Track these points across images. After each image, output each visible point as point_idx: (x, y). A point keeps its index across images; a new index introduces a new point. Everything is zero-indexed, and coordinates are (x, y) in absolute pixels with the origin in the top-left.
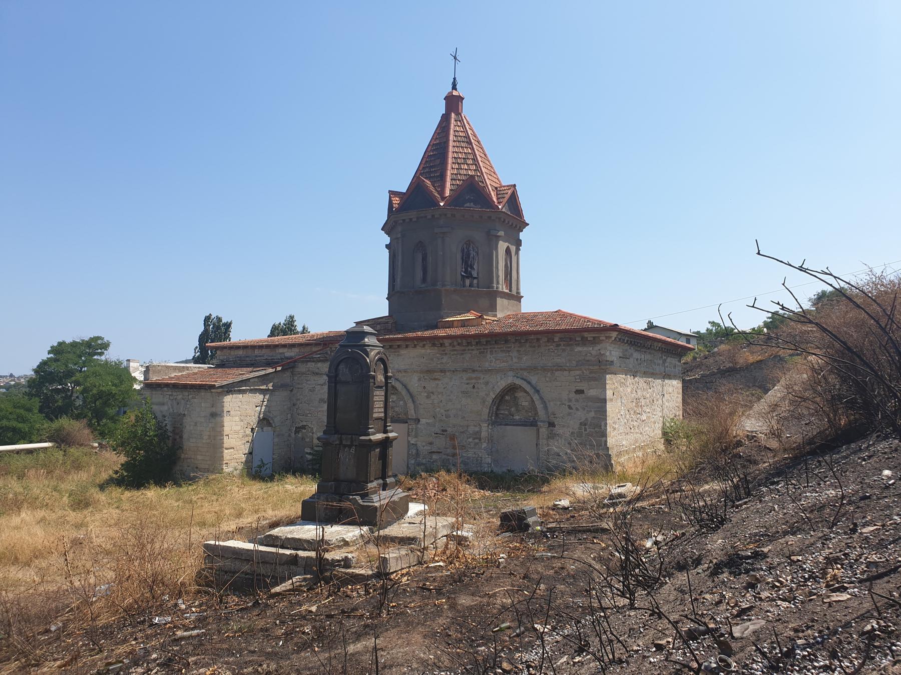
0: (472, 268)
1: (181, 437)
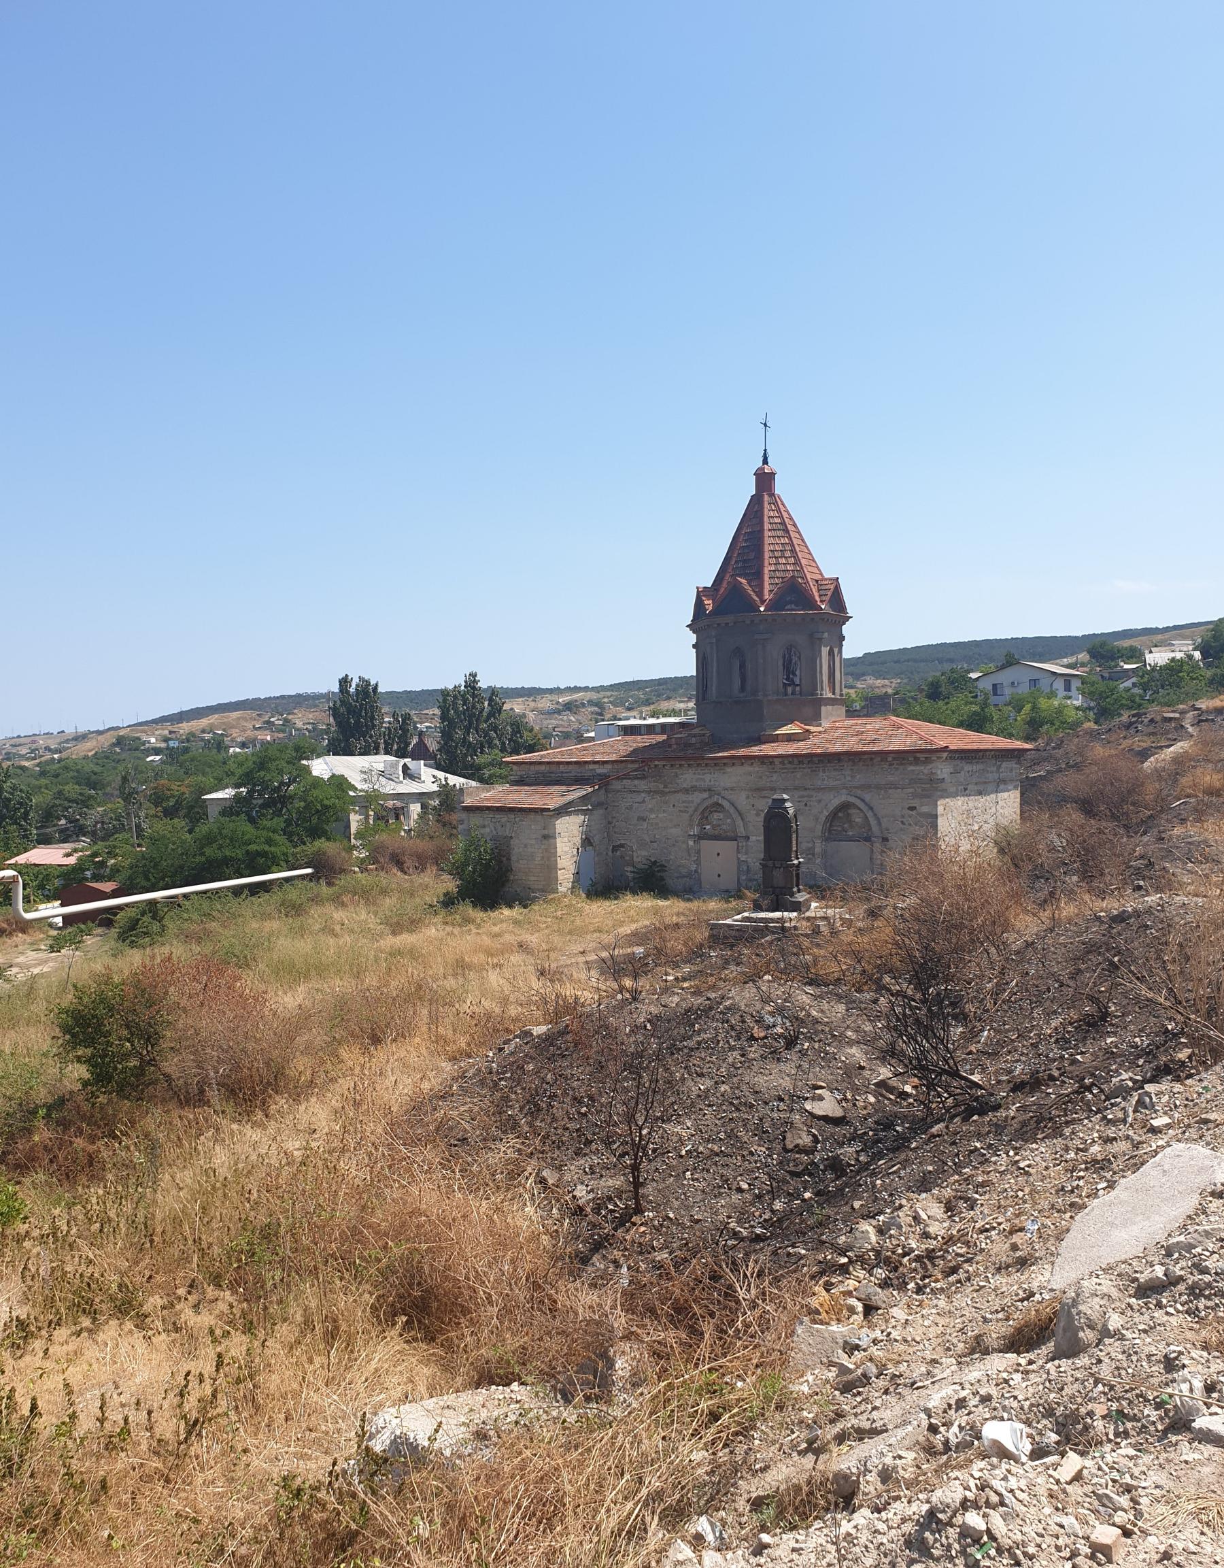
0: (795, 675)
1: (509, 859)
